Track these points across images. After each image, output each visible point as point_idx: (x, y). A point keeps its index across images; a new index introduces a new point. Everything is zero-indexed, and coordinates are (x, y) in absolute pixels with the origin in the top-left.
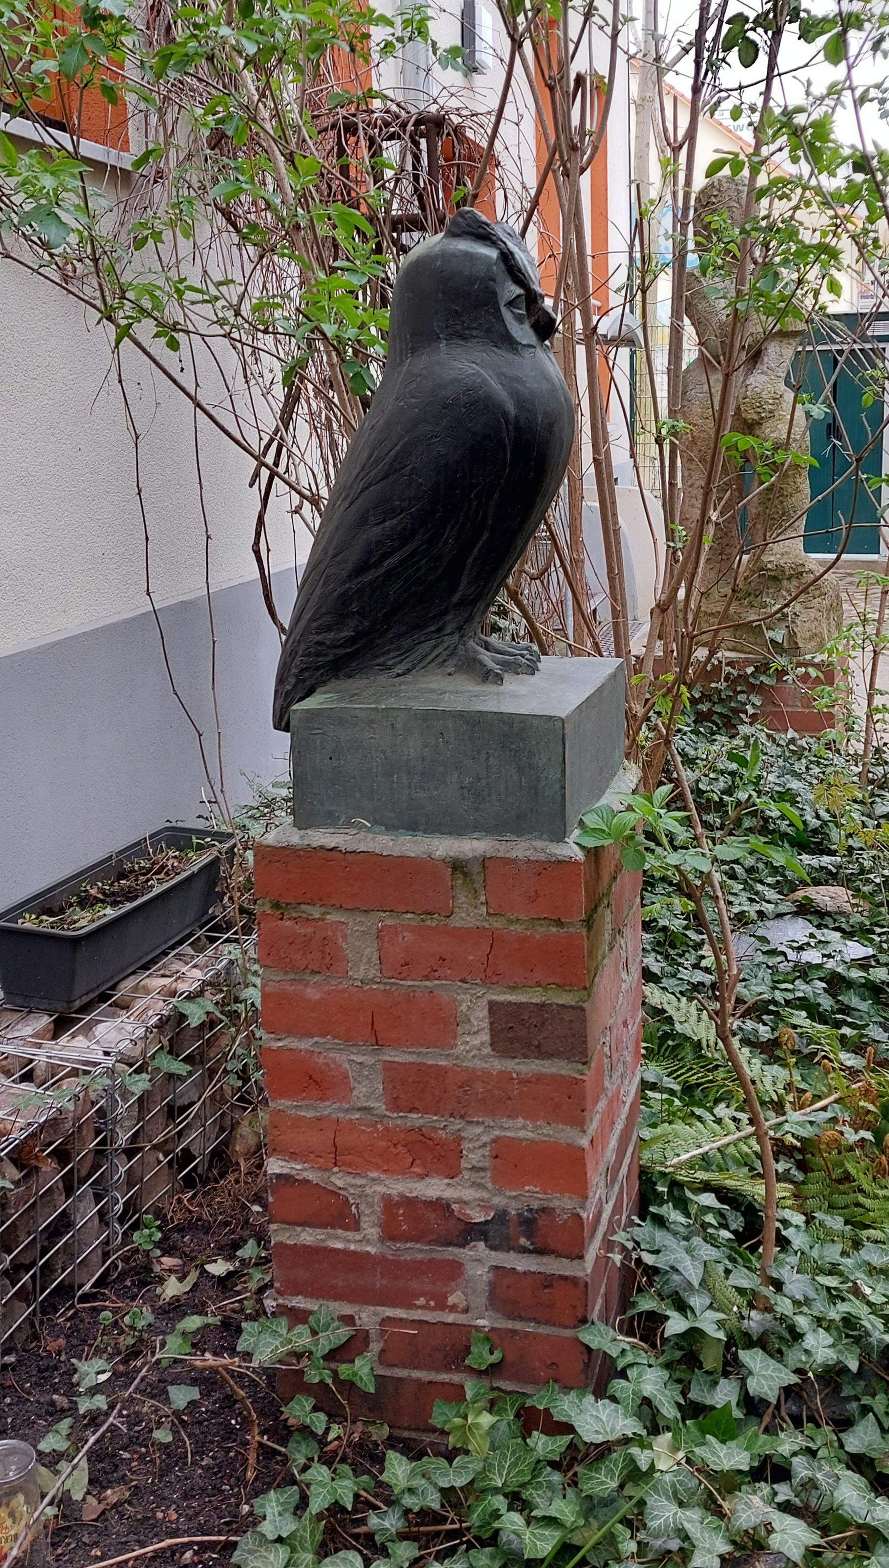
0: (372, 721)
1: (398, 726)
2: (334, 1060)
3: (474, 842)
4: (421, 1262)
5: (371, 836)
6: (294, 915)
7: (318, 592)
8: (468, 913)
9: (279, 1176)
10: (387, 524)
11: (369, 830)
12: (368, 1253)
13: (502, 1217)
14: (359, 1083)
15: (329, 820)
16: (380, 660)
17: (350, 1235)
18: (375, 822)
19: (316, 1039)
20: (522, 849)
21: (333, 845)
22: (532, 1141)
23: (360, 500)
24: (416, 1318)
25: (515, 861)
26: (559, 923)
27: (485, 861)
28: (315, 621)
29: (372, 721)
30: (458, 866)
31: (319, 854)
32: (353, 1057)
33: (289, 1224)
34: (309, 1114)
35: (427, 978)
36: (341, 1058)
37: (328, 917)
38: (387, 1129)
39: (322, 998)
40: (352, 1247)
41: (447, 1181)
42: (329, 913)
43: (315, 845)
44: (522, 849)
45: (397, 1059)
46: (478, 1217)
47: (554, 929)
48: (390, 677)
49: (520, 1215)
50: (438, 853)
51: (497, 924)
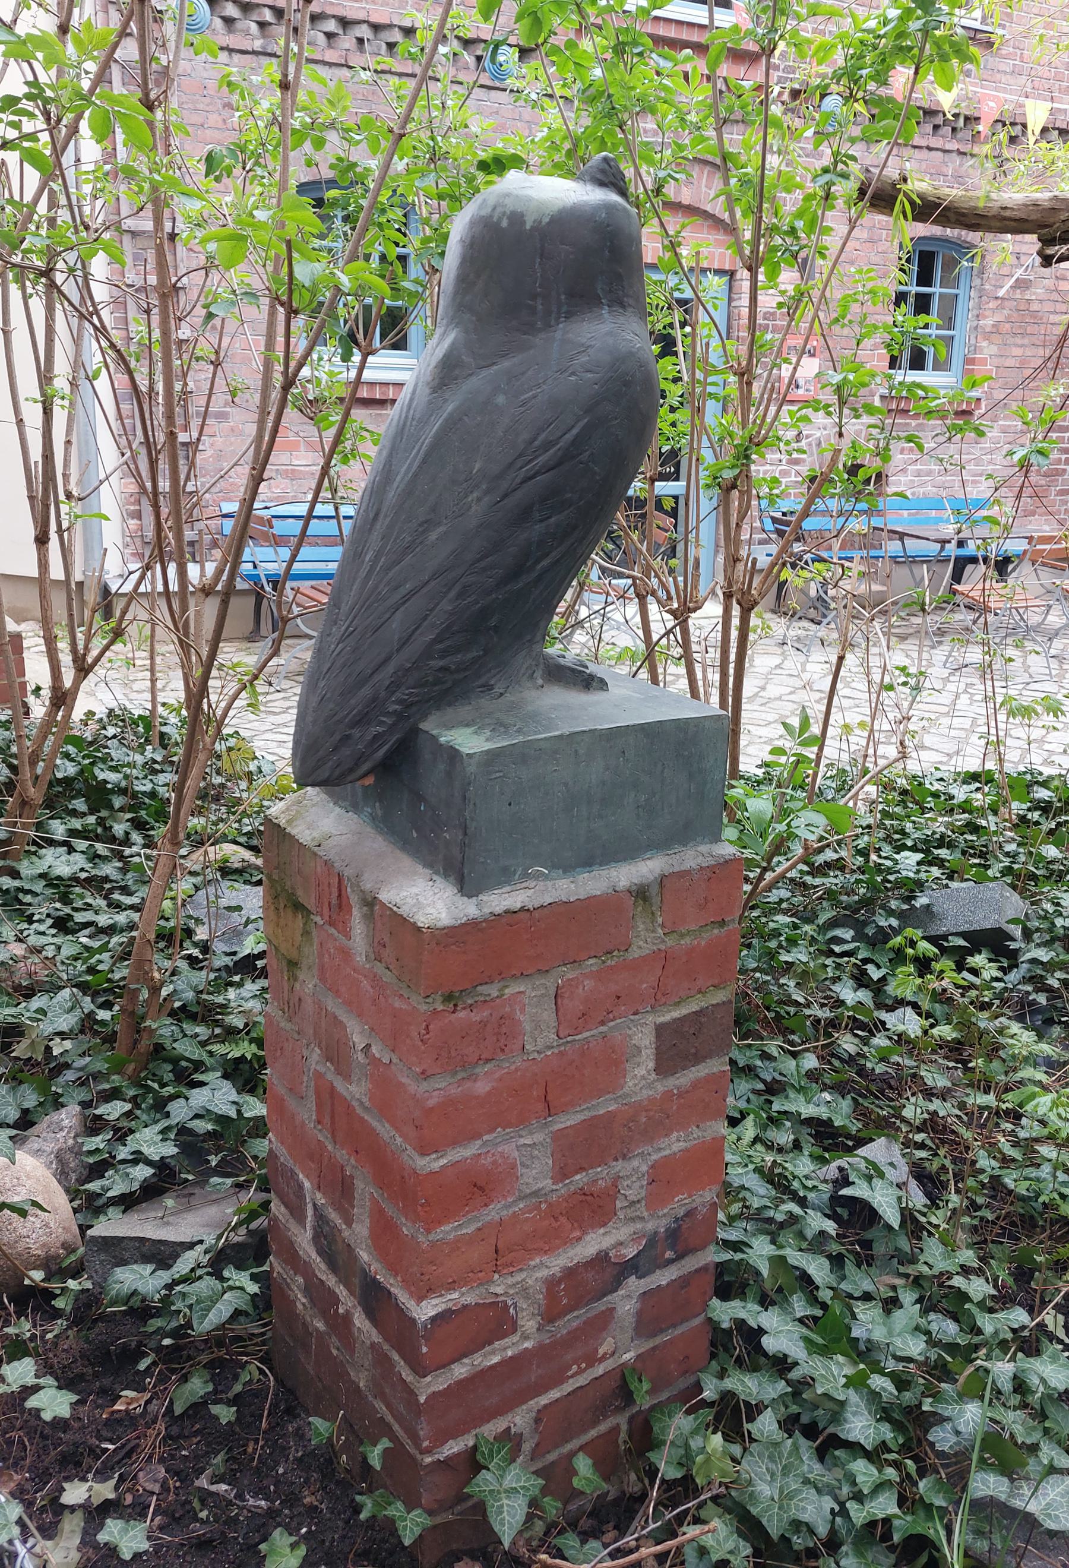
0: (556, 752)
1: (581, 752)
2: (502, 1154)
3: (648, 862)
4: (577, 1329)
5: (549, 883)
6: (470, 1002)
7: (446, 606)
8: (645, 940)
9: (434, 1319)
10: (553, 520)
11: (546, 877)
12: (526, 1349)
13: (653, 1240)
14: (527, 1167)
15: (505, 877)
16: (482, 681)
17: (515, 1338)
18: (553, 867)
19: (485, 1138)
20: (692, 857)
21: (519, 906)
22: (685, 1151)
23: (519, 494)
24: (570, 1389)
25: (687, 873)
26: (723, 923)
27: (663, 880)
28: (440, 642)
29: (556, 752)
30: (641, 893)
31: (504, 920)
32: (522, 1141)
33: (444, 1366)
34: (469, 1230)
35: (603, 1023)
36: (508, 1149)
37: (507, 991)
38: (550, 1205)
39: (493, 1088)
40: (510, 1353)
41: (602, 1231)
42: (507, 987)
43: (498, 910)
44: (692, 857)
45: (568, 1124)
46: (630, 1252)
47: (716, 931)
48: (493, 698)
49: (667, 1230)
50: (622, 884)
51: (670, 942)
